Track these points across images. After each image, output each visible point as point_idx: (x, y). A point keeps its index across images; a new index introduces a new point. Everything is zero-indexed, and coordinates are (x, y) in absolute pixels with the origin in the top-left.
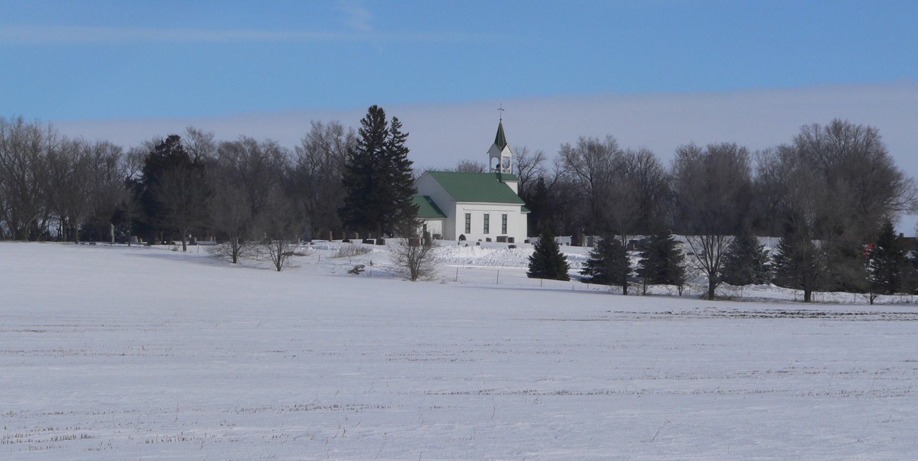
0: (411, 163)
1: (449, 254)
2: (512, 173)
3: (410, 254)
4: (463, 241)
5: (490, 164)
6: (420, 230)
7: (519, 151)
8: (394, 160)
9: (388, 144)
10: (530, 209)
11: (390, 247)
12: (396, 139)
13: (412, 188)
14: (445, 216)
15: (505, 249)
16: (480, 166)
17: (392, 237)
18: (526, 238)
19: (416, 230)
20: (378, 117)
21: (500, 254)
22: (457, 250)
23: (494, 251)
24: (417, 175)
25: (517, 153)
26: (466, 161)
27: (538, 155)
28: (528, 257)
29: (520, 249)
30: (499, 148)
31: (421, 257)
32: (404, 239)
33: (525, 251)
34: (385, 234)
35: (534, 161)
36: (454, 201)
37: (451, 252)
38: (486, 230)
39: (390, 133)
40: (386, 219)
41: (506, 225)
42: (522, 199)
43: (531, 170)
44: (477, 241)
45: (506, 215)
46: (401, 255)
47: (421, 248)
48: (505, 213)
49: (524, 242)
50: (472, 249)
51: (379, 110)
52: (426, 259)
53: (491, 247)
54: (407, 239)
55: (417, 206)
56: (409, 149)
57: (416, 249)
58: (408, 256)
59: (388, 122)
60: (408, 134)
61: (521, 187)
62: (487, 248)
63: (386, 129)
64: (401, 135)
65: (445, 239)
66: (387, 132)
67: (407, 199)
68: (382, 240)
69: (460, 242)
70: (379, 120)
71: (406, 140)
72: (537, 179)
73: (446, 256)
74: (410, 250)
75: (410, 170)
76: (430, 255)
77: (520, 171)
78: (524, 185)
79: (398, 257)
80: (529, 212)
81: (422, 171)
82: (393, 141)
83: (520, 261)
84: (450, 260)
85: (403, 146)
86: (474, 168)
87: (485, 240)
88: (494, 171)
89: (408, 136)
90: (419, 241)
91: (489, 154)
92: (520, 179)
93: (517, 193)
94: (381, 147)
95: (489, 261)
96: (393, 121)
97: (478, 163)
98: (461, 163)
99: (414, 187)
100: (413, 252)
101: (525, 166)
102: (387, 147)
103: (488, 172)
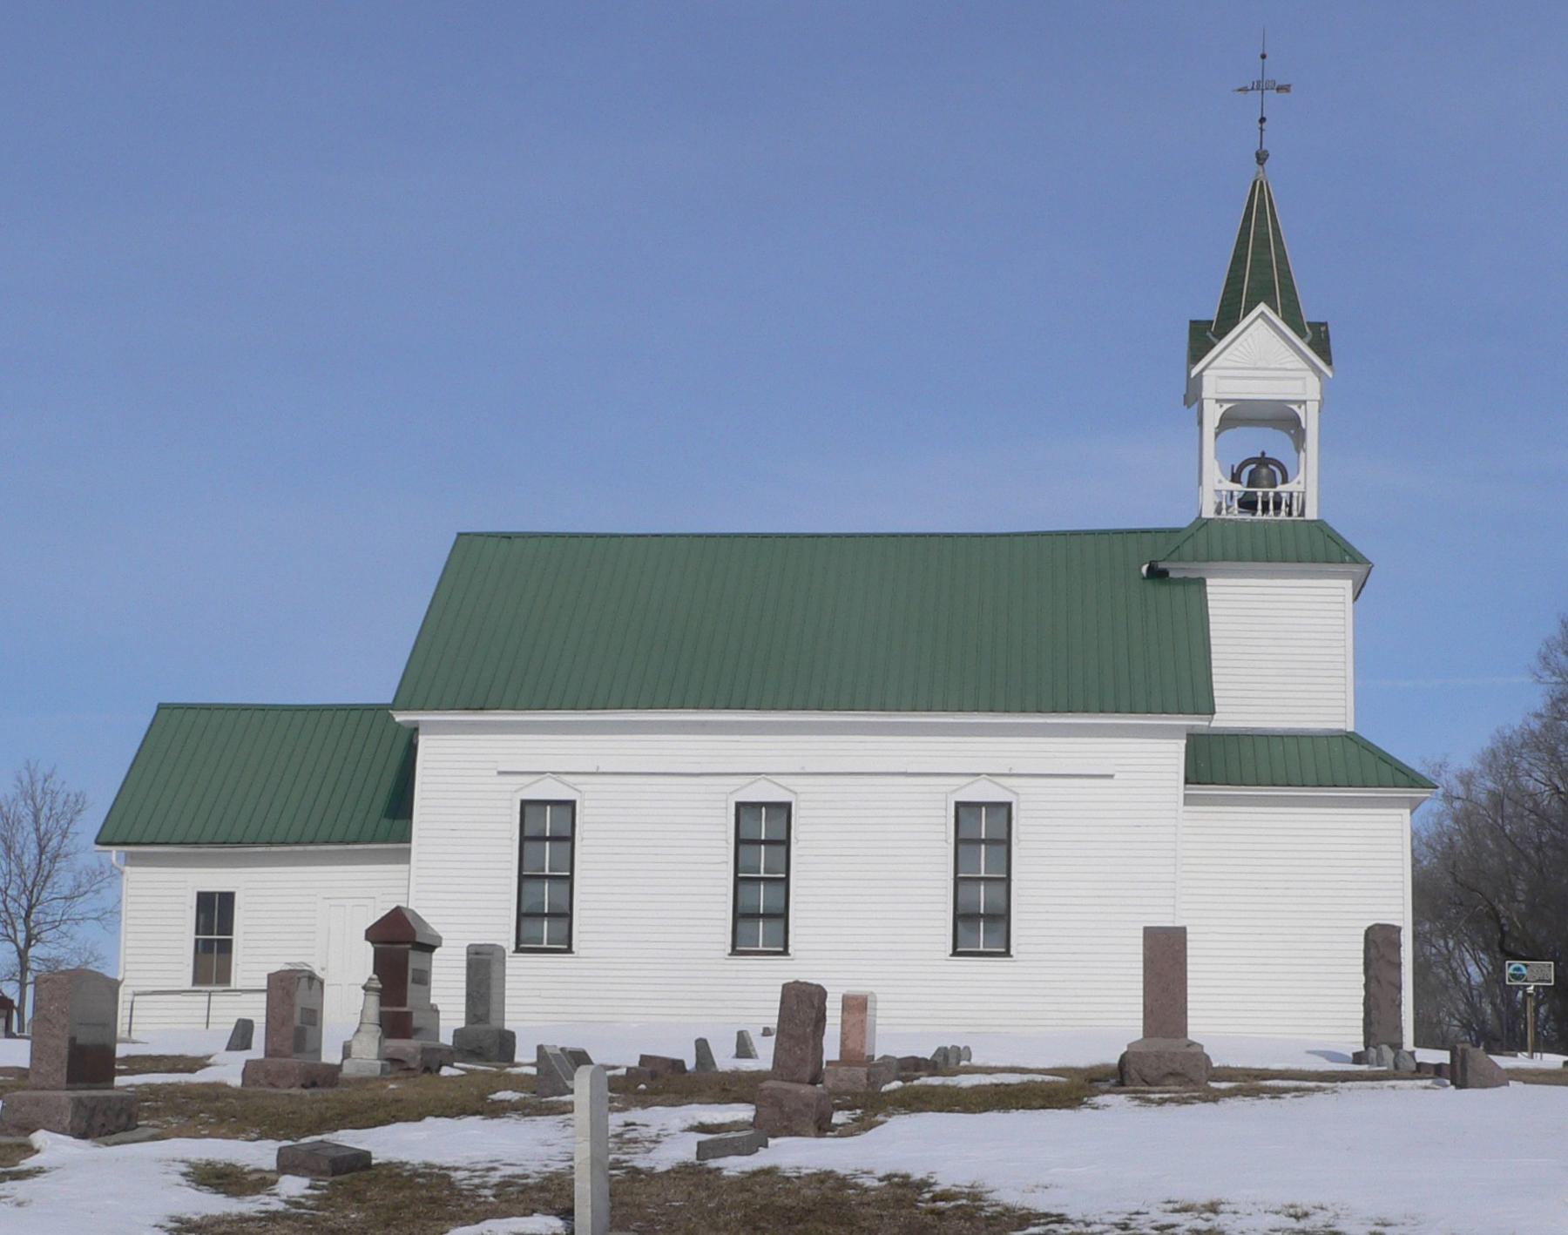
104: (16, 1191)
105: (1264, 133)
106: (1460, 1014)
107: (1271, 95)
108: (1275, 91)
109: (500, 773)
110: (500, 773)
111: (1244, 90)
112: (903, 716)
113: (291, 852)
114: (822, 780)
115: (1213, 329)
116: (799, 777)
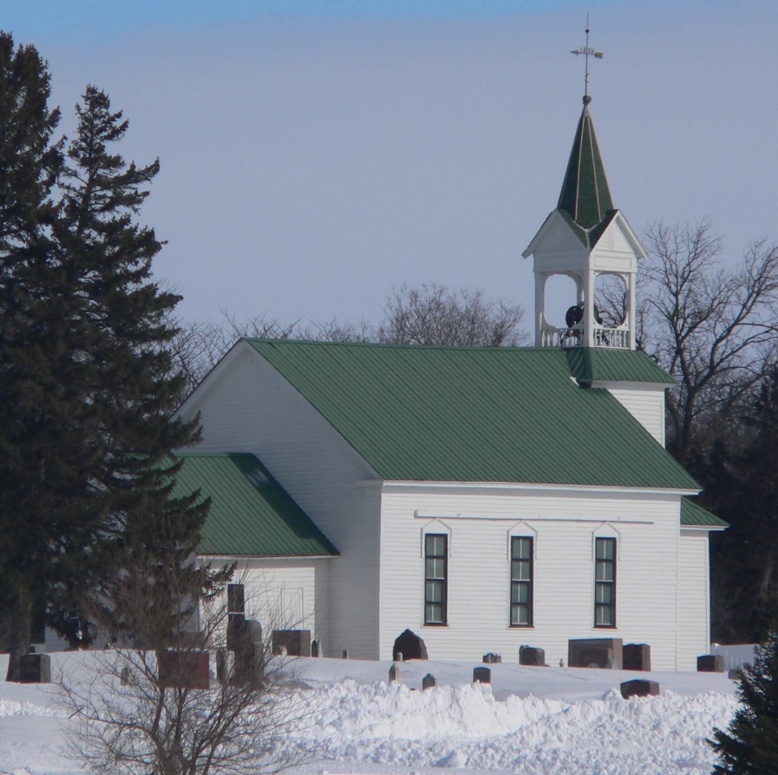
0: (171, 300)
1: (346, 724)
2: (639, 348)
3: (162, 724)
4: (413, 661)
5: (539, 306)
6: (208, 610)
7: (671, 247)
8: (94, 289)
9: (63, 215)
10: (722, 514)
11: (69, 691)
12: (98, 191)
13: (173, 420)
14: (332, 549)
15: (603, 698)
16: (493, 316)
17: (86, 643)
18: (705, 648)
19: (192, 611)
20: (15, 92)
21: (582, 724)
22: (383, 702)
23: (555, 706)
24: (205, 356)
25: (665, 256)
26: (431, 294)
27: (759, 264)
28: (711, 738)
29: (676, 698)
30: (581, 234)
31: (214, 737)
32: (135, 655)
33: (697, 708)
34: (50, 633)
35: (744, 292)
36: (371, 478)
37: (354, 716)
38: (519, 610)
39: (70, 163)
40: (55, 560)
41: (611, 586)
42: (688, 468)
43: (729, 330)
44: (479, 662)
45: (530, 540)
46: (122, 725)
47: (215, 695)
48: (606, 532)
49: (695, 665)
50: (455, 699)
51: (20, 55)
52: (235, 749)
53: (544, 692)
54: (152, 656)
55: (199, 501)
56: (158, 238)
57: (191, 702)
58: (153, 732)
59: (64, 115)
60: (155, 169)
61: (681, 412)
62: (522, 695)
63: (53, 141)
64: (122, 172)
65: (329, 654)
66: (61, 159)
67: (155, 466)
68: (38, 658)
69: (401, 665)
70: (20, 101)
71: (146, 194)
72: (758, 377)
73: (331, 730)
74: (161, 704)
75: (164, 334)
76: (255, 730)
77: (679, 339)
78: (697, 401)
79: (108, 735)
80: (721, 528)
81: (228, 338)
82: (86, 198)
83: (677, 756)
84: (349, 752)
85: (133, 224)
86: (465, 323)
87: (511, 656)
88: (555, 338)
89: (156, 179)
90: (207, 657)
91: (531, 258)
92: (679, 376)
93: (664, 446)
94: (30, 228)
95: (530, 755)
96: (85, 107)
97: (484, 302)
98: (406, 302)
99: (184, 413)
100: (174, 714)
101: (700, 316)
102: (60, 230)
103: (530, 342)
104: (620, 715)
105: (588, 84)
106: (215, 712)
107: (591, 58)
108: (594, 56)
109: (651, 523)
110: (651, 523)
111: (576, 52)
112: (675, 491)
113: (281, 560)
114: (472, 522)
115: (576, 219)
116: (535, 521)
